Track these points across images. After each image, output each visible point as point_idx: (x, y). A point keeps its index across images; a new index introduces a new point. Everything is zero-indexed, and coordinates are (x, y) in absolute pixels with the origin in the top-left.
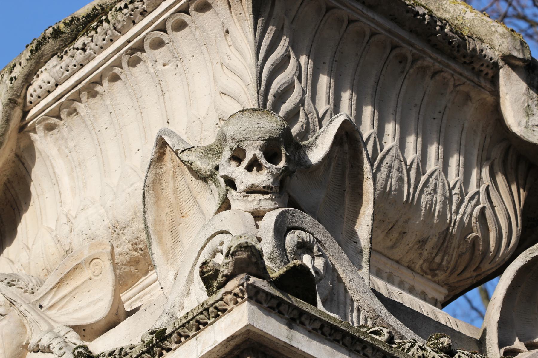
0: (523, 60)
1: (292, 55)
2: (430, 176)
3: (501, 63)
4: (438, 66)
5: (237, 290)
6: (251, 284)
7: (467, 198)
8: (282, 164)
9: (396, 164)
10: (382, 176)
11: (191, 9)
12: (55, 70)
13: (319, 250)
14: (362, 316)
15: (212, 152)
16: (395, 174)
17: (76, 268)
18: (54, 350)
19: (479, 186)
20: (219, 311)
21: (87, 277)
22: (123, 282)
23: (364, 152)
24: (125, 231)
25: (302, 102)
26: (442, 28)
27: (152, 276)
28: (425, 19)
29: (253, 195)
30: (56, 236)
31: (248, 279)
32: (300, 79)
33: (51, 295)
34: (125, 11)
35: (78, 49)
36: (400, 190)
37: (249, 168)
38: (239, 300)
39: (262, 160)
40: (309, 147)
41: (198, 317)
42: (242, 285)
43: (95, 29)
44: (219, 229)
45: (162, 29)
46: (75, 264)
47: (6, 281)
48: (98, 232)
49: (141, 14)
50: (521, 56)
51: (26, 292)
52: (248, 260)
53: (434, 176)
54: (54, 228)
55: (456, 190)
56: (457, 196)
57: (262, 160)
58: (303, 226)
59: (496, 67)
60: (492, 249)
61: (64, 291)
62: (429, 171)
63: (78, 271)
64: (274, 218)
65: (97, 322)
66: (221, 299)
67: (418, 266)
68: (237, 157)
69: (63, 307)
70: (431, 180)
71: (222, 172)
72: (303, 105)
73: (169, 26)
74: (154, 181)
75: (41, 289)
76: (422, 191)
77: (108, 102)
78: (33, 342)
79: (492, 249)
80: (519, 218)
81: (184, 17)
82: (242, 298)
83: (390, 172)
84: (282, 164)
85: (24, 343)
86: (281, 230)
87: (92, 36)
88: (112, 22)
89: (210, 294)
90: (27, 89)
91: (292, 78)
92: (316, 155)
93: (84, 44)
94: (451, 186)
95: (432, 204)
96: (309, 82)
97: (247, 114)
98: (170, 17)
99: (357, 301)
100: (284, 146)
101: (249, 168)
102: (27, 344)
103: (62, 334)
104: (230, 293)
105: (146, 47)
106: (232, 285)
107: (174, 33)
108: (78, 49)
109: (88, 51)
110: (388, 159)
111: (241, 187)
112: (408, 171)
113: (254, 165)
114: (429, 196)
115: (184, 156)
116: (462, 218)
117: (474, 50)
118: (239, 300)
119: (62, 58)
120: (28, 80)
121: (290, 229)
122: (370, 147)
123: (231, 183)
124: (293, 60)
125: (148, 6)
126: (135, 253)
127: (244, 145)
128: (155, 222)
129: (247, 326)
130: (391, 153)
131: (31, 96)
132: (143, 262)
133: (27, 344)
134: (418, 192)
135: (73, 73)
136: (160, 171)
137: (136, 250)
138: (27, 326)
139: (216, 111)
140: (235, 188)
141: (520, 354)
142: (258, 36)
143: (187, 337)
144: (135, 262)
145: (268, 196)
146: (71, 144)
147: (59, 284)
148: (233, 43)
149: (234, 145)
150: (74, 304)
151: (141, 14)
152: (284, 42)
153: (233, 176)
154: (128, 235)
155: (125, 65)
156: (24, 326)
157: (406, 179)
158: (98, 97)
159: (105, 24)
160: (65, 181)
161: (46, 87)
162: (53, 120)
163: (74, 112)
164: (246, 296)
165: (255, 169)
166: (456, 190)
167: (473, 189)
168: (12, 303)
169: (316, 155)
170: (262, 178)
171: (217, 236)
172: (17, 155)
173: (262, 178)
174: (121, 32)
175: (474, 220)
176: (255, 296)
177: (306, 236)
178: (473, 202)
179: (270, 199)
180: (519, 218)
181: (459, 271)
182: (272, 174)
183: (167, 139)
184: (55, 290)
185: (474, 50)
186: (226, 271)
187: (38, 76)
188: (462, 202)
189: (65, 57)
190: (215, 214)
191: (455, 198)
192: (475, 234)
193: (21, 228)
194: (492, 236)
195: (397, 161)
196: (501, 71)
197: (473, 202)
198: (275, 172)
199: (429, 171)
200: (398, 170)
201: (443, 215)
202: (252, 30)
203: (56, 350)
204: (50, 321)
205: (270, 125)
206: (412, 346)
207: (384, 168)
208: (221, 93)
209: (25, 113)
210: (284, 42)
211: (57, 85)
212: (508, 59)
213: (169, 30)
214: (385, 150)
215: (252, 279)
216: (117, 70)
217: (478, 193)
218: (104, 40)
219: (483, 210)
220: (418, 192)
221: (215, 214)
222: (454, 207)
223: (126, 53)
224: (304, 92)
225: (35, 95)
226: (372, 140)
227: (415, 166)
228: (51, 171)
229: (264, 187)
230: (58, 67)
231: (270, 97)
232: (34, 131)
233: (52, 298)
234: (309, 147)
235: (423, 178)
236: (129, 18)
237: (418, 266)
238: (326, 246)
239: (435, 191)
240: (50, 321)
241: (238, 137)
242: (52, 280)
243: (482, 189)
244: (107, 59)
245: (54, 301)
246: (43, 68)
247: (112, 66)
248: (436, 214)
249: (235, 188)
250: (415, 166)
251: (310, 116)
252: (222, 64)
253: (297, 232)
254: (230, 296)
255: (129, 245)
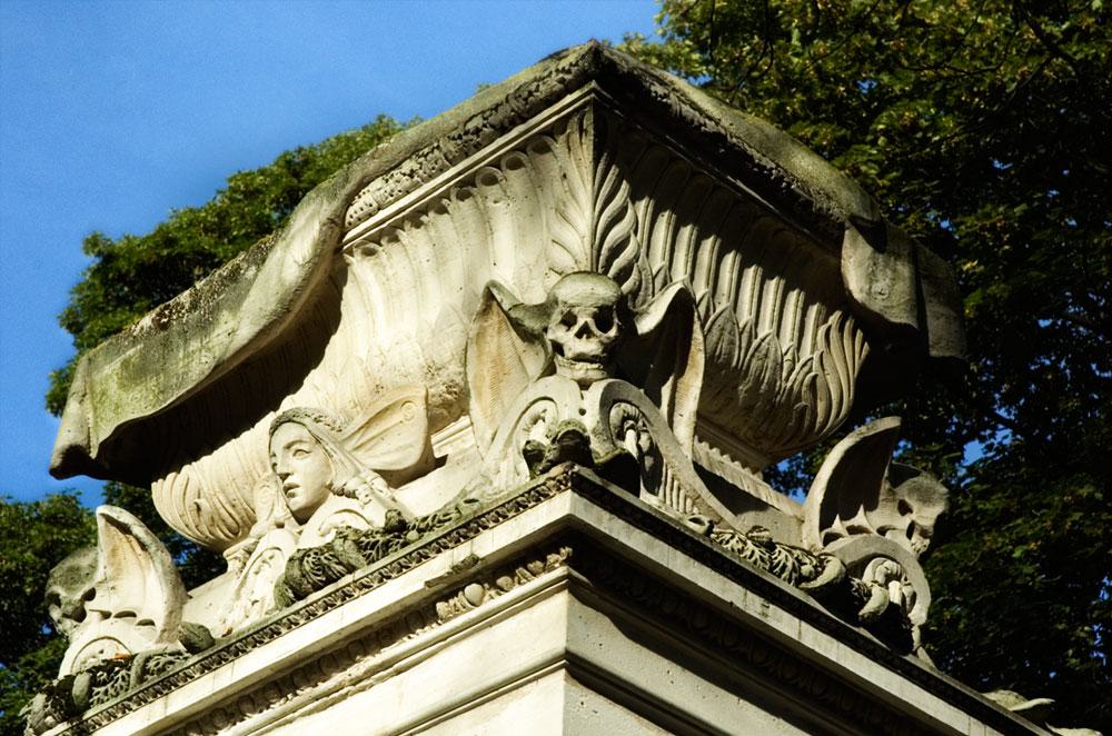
0: (871, 222)
1: (630, 205)
2: (763, 340)
3: (847, 224)
4: (781, 225)
5: (561, 477)
6: (576, 473)
7: (798, 367)
8: (613, 333)
9: (728, 327)
10: (713, 337)
11: (528, 148)
12: (378, 193)
13: (644, 425)
14: (682, 495)
15: (544, 310)
16: (726, 336)
17: (387, 409)
18: (360, 497)
19: (812, 352)
20: (538, 495)
21: (398, 421)
22: (435, 422)
23: (696, 314)
24: (440, 372)
25: (636, 258)
26: (789, 184)
27: (464, 420)
28: (772, 174)
29: (581, 364)
30: (366, 368)
31: (572, 467)
32: (636, 232)
33: (358, 435)
34: (459, 142)
35: (404, 175)
36: (730, 355)
37: (579, 335)
38: (562, 487)
39: (593, 328)
40: (641, 314)
41: (519, 499)
42: (567, 473)
43: (425, 156)
44: (543, 396)
45: (496, 164)
46: (386, 404)
47: (313, 417)
48: (411, 371)
49: (475, 146)
50: (870, 218)
51: (333, 429)
52: (573, 446)
53: (766, 341)
54: (364, 359)
55: (789, 356)
56: (789, 363)
57: (593, 328)
58: (630, 399)
59: (842, 228)
60: (818, 425)
61: (369, 435)
62: (761, 336)
63: (388, 412)
64: (601, 390)
65: (405, 469)
66: (544, 484)
67: (742, 434)
68: (569, 320)
69: (370, 449)
70: (763, 344)
71: (550, 336)
72: (637, 261)
73: (503, 163)
74: (478, 334)
75: (349, 428)
76: (753, 356)
77: (432, 233)
78: (337, 485)
79: (818, 425)
80: (852, 388)
81: (523, 157)
82: (566, 485)
83: (721, 334)
84: (613, 333)
85: (328, 483)
86: (607, 403)
87: (421, 164)
88: (444, 150)
89: (532, 478)
90: (347, 210)
91: (629, 232)
92: (646, 325)
93: (412, 171)
94: (784, 352)
95: (762, 369)
96: (646, 236)
97: (583, 275)
98: (505, 154)
99: (679, 480)
100: (618, 312)
101: (579, 335)
102: (331, 485)
103: (368, 480)
104: (554, 479)
105: (478, 182)
106: (556, 471)
107: (508, 171)
108: (404, 175)
109: (416, 178)
110: (720, 321)
111: (569, 354)
112: (741, 334)
113: (584, 332)
114: (760, 362)
115: (513, 314)
116: (792, 386)
117: (821, 209)
118: (562, 487)
119: (387, 181)
120: (349, 202)
121: (615, 402)
122: (702, 309)
123: (558, 348)
124: (630, 211)
125: (483, 140)
126: (449, 397)
127: (575, 311)
128: (475, 377)
129: (568, 515)
130: (724, 315)
131: (351, 217)
132: (456, 406)
133: (331, 485)
134: (748, 357)
135: (397, 199)
136: (486, 324)
137: (450, 393)
138: (332, 466)
139: (547, 260)
140: (563, 355)
141: (841, 539)
142: (596, 186)
143: (505, 517)
144: (446, 405)
145: (596, 366)
146: (390, 272)
147: (368, 424)
148: (570, 189)
149: (566, 310)
150: (382, 447)
151: (475, 146)
152: (614, 170)
153: (561, 341)
154: (443, 377)
155: (453, 197)
156: (328, 466)
157: (738, 343)
158: (423, 227)
159: (436, 152)
160: (380, 308)
161: (366, 209)
162: (372, 245)
163: (396, 239)
164: (569, 485)
165: (585, 336)
166: (789, 356)
167: (806, 354)
168: (318, 441)
169: (646, 325)
170: (591, 346)
171: (540, 402)
172: (330, 277)
173: (591, 346)
174: (453, 163)
175: (804, 389)
176: (580, 486)
177: (631, 410)
178: (806, 369)
179: (598, 369)
180: (852, 388)
181: (785, 440)
182: (602, 343)
183: (495, 292)
184: (362, 431)
185: (821, 209)
186: (550, 456)
187: (360, 197)
188: (793, 370)
189: (390, 181)
190: (539, 378)
191: (786, 365)
192: (804, 403)
193: (329, 350)
194: (821, 407)
195: (730, 324)
196: (847, 232)
197: (806, 369)
198: (606, 341)
199: (761, 336)
200: (730, 333)
201: (772, 383)
202: (590, 178)
203: (361, 497)
204: (356, 462)
205: (604, 291)
206: (732, 538)
207: (715, 331)
208: (554, 241)
209: (343, 235)
210: (614, 170)
211: (379, 209)
212: (854, 220)
213: (504, 168)
214: (718, 311)
215: (577, 468)
216: (445, 201)
217: (812, 358)
218: (433, 168)
219: (815, 377)
220: (748, 357)
221: (539, 378)
222: (784, 374)
223: (456, 185)
224: (639, 247)
225: (355, 216)
226: (706, 300)
227: (747, 329)
228: (365, 298)
229: (593, 356)
230: (382, 191)
231: (604, 252)
232: (351, 253)
233: (359, 440)
234: (641, 314)
235: (755, 343)
236: (461, 150)
237: (742, 434)
238: (651, 420)
239: (766, 356)
240: (356, 462)
241: (571, 302)
242: (360, 420)
243: (816, 356)
244: (435, 189)
245: (361, 442)
246: (366, 189)
247: (440, 197)
248: (766, 381)
249: (563, 355)
250: (747, 329)
251: (643, 273)
252: (556, 210)
253: (623, 405)
254: (552, 482)
255: (444, 388)
